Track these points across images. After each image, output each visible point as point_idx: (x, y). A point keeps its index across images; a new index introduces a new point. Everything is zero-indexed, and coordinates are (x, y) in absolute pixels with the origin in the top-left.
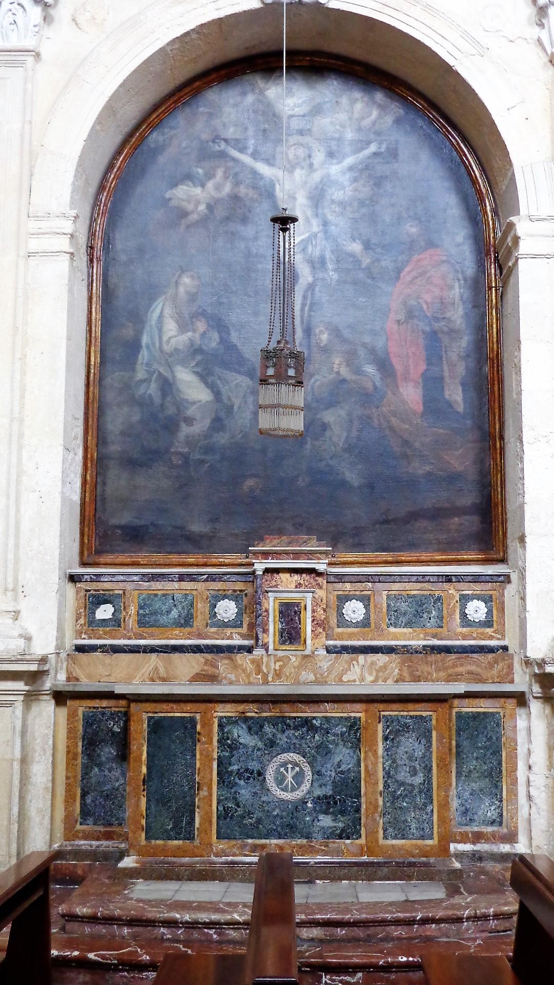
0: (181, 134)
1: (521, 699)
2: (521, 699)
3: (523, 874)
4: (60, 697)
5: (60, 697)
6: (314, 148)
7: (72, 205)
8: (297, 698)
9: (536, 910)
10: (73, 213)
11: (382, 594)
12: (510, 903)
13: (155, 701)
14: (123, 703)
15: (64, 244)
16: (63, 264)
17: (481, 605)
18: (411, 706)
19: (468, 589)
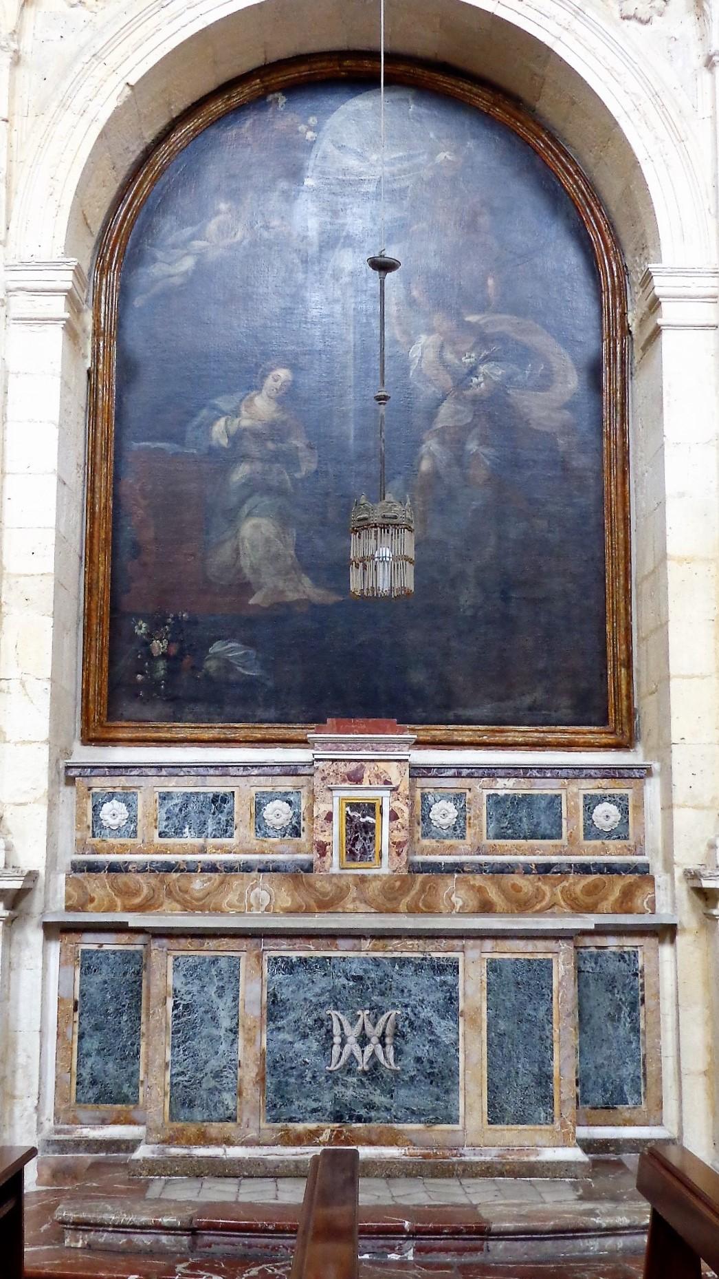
0: (245, 143)
1: (667, 932)
2: (667, 932)
3: (660, 1172)
4: (54, 930)
5: (54, 930)
6: (368, 161)
7: (69, 250)
8: (179, 932)
9: (675, 1220)
10: (74, 261)
11: (148, 790)
12: (640, 1212)
13: (419, 937)
14: (140, 938)
15: (58, 307)
16: (55, 336)
17: (107, 807)
18: (299, 943)
19: (265, 784)
